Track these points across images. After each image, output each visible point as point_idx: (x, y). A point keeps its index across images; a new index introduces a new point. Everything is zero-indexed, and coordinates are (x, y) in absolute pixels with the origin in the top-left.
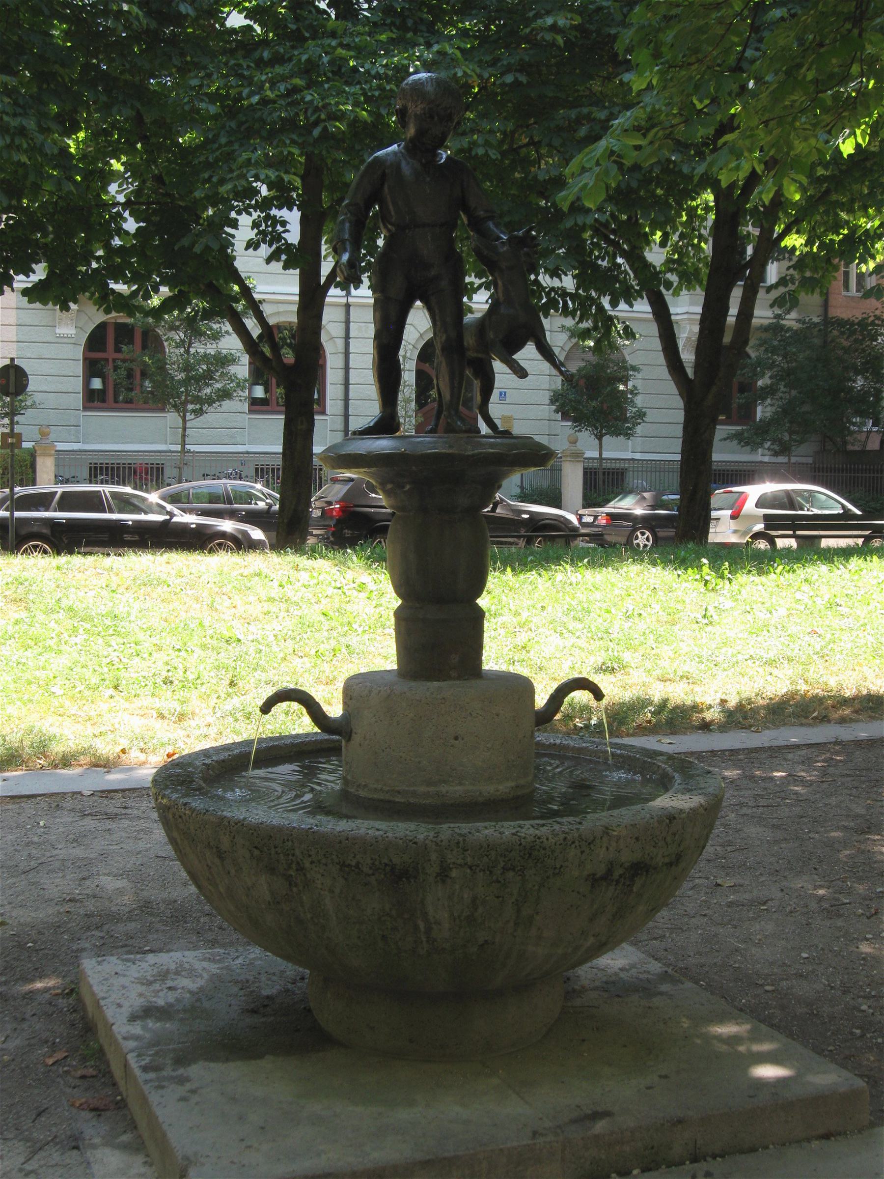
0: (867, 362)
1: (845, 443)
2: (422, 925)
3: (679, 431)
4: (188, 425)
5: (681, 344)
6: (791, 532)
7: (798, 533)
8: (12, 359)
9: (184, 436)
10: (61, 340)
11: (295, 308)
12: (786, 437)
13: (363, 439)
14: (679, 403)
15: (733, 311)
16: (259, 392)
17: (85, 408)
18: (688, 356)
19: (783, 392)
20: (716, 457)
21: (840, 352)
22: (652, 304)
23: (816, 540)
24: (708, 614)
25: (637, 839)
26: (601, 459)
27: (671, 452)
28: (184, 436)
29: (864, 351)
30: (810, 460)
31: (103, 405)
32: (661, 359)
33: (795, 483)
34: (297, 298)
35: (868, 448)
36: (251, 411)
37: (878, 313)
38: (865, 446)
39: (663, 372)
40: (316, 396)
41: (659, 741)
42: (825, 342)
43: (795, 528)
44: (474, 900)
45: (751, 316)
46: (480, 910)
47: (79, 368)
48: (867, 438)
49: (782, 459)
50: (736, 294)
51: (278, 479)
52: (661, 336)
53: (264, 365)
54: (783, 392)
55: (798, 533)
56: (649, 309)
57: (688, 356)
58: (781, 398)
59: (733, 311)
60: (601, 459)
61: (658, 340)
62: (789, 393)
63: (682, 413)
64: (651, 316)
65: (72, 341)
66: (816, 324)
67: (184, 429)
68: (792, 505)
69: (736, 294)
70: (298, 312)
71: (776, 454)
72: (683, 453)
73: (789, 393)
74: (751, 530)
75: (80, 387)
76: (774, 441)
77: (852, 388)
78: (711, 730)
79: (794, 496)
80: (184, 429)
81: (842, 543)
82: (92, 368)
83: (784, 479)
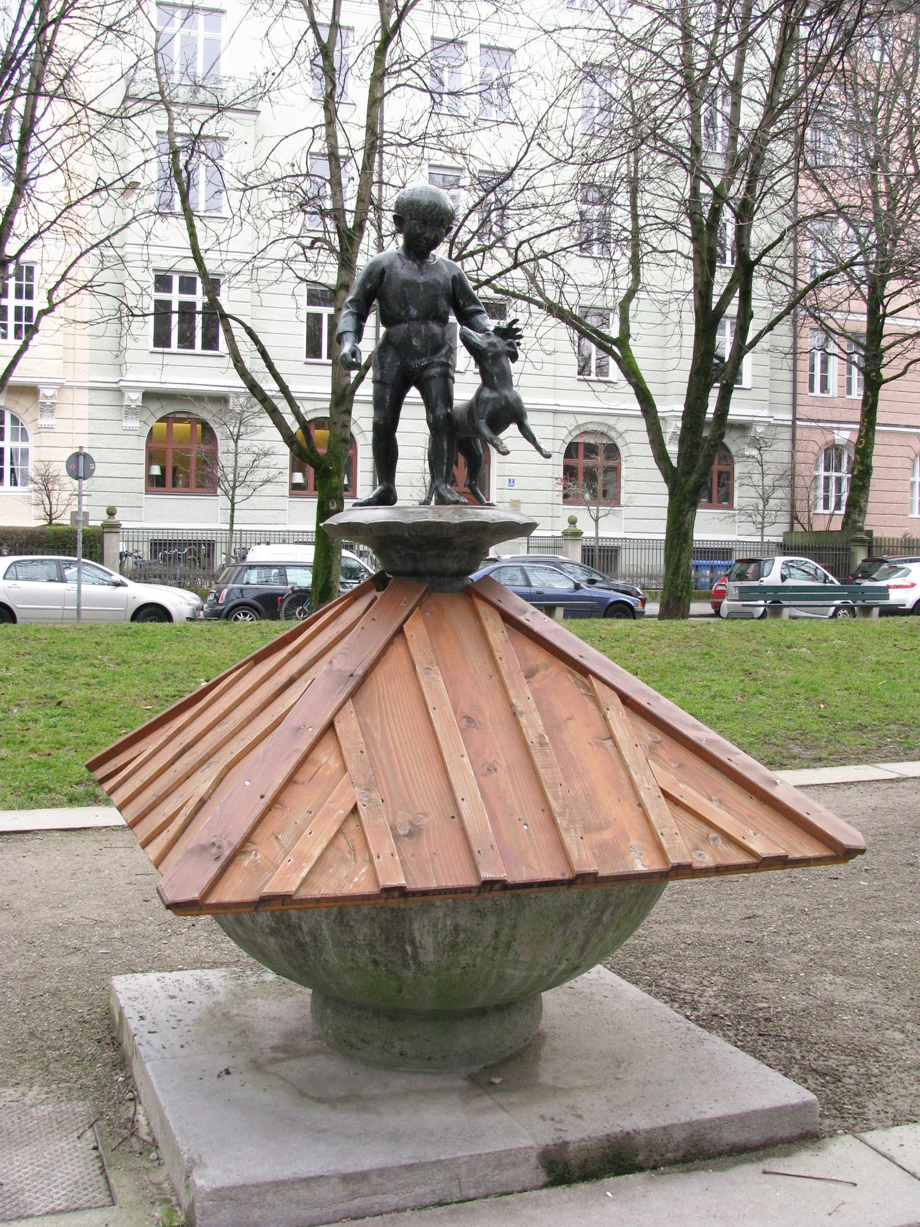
2: (409, 949)
3: (664, 514)
4: (236, 506)
5: (666, 438)
8: (81, 448)
9: (232, 517)
10: (128, 432)
11: (328, 405)
14: (664, 488)
15: (711, 409)
16: (299, 478)
17: (148, 492)
18: (672, 449)
20: (697, 536)
25: (142, 1018)
26: (597, 538)
27: (658, 531)
28: (232, 517)
31: (187, 490)
32: (649, 451)
34: (330, 397)
36: (291, 495)
39: (652, 463)
40: (346, 482)
44: (456, 928)
45: (726, 412)
46: (462, 936)
47: (142, 458)
50: (714, 395)
51: (838, 506)
52: (648, 430)
53: (303, 453)
56: (638, 407)
57: (672, 449)
59: (711, 409)
60: (597, 538)
61: (399, 443)
63: (667, 497)
64: (640, 413)
65: (137, 433)
67: (233, 510)
69: (714, 395)
70: (331, 408)
72: (667, 533)
75: (143, 475)
80: (233, 510)
81: (804, 614)
82: (152, 457)
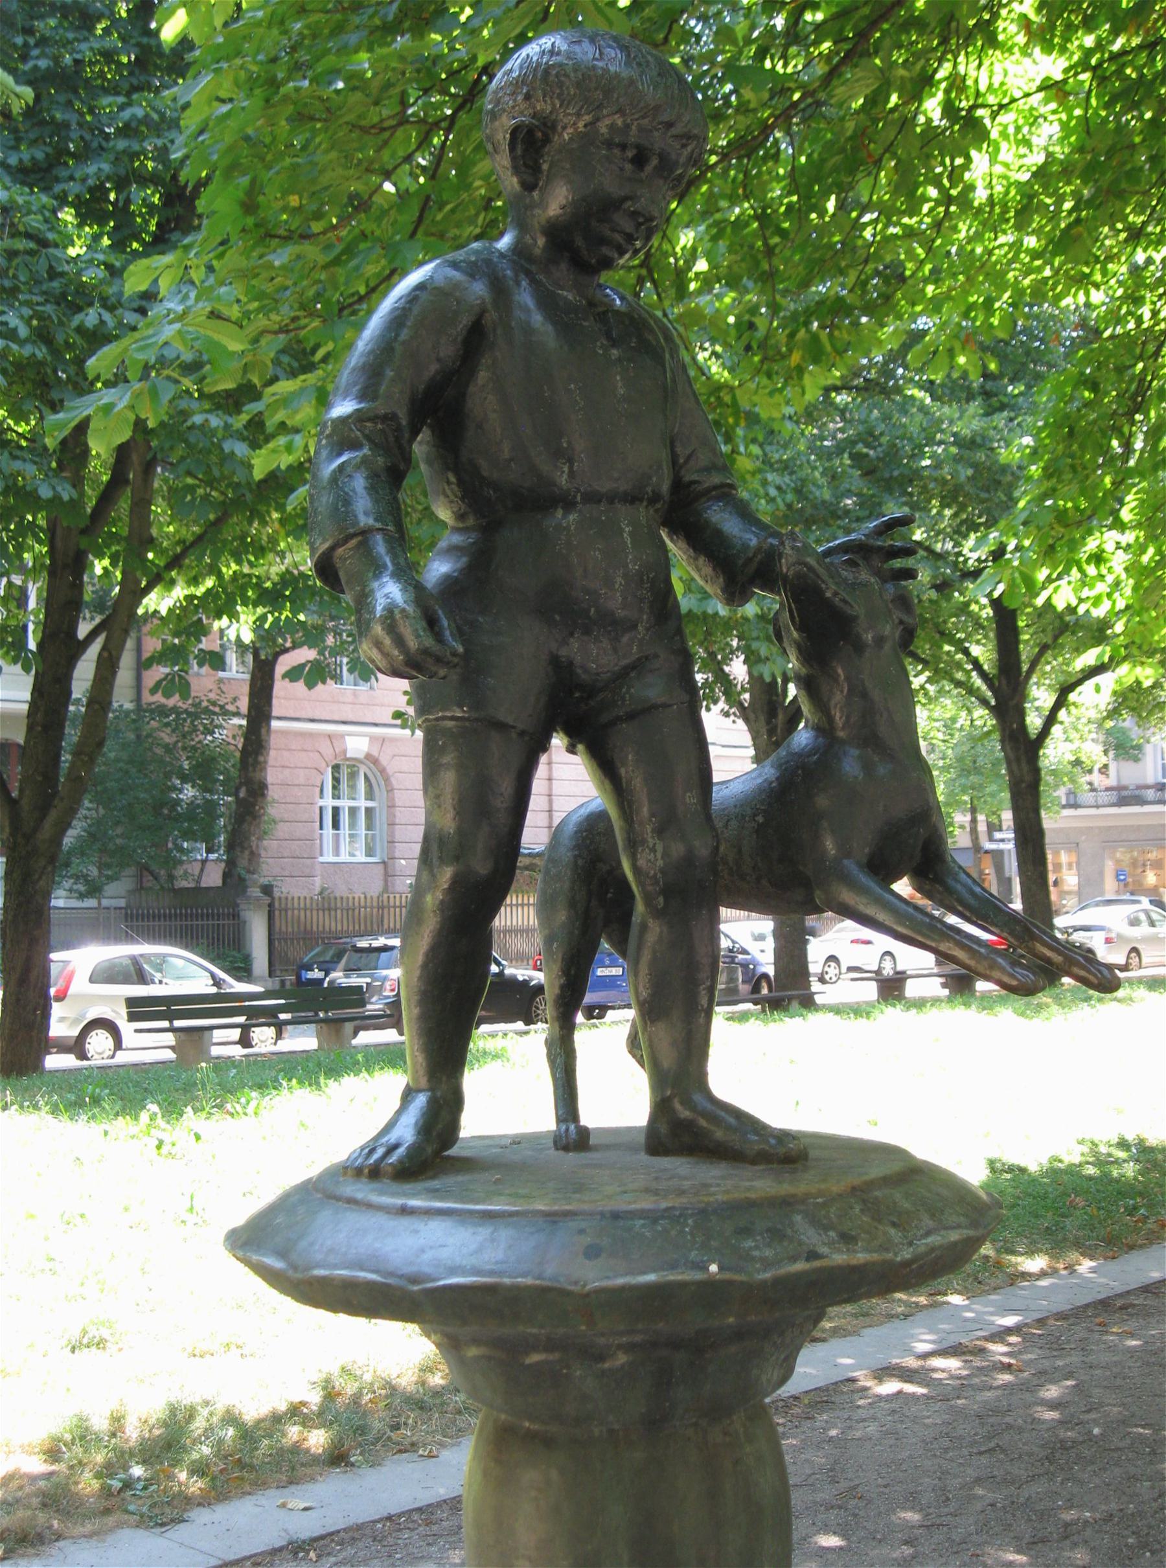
0: (199, 765)
1: (171, 878)
6: (165, 1024)
7: (178, 1023)
12: (94, 872)
13: (491, 1273)
19: (89, 809)
21: (159, 751)
22: (37, 690)
23: (207, 1033)
24: (197, 1207)
29: (194, 748)
30: (122, 903)
33: (138, 943)
35: (203, 885)
37: (212, 696)
38: (198, 882)
41: (283, 1505)
42: (138, 737)
43: (170, 1016)
48: (202, 870)
49: (92, 903)
54: (89, 809)
55: (178, 1023)
58: (86, 818)
62: (97, 810)
66: (127, 713)
68: (142, 978)
71: (82, 896)
73: (97, 810)
74: (84, 1016)
76: (77, 877)
77: (178, 802)
78: (353, 1465)
79: (142, 960)
83: (128, 939)
